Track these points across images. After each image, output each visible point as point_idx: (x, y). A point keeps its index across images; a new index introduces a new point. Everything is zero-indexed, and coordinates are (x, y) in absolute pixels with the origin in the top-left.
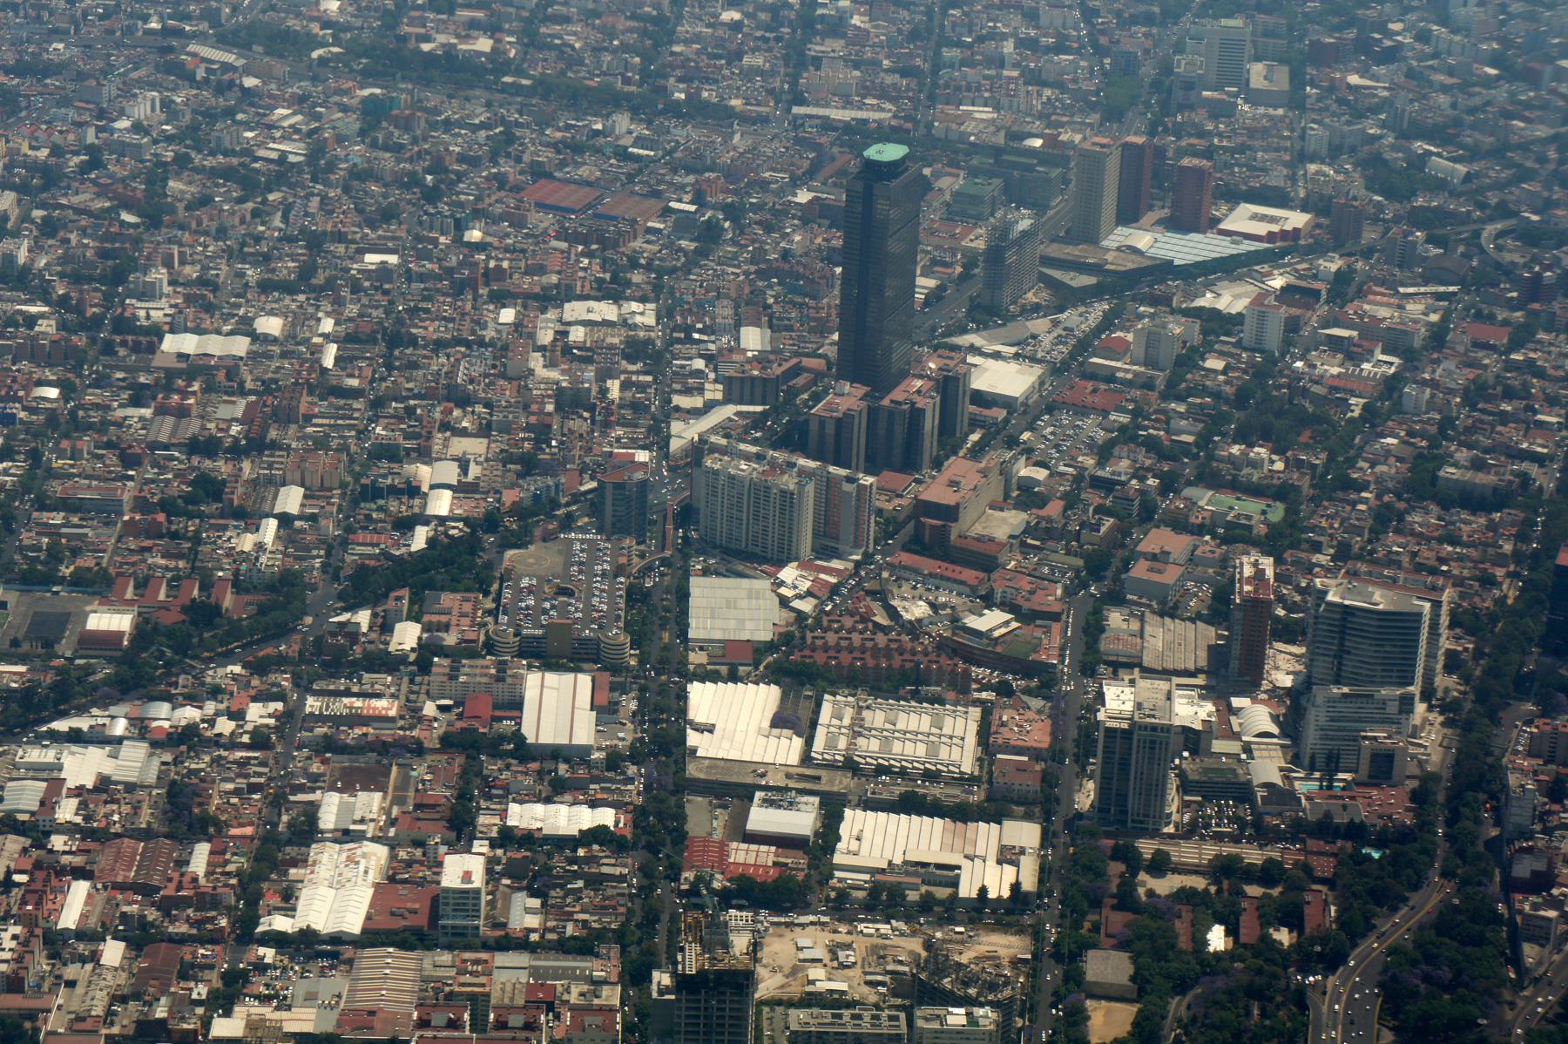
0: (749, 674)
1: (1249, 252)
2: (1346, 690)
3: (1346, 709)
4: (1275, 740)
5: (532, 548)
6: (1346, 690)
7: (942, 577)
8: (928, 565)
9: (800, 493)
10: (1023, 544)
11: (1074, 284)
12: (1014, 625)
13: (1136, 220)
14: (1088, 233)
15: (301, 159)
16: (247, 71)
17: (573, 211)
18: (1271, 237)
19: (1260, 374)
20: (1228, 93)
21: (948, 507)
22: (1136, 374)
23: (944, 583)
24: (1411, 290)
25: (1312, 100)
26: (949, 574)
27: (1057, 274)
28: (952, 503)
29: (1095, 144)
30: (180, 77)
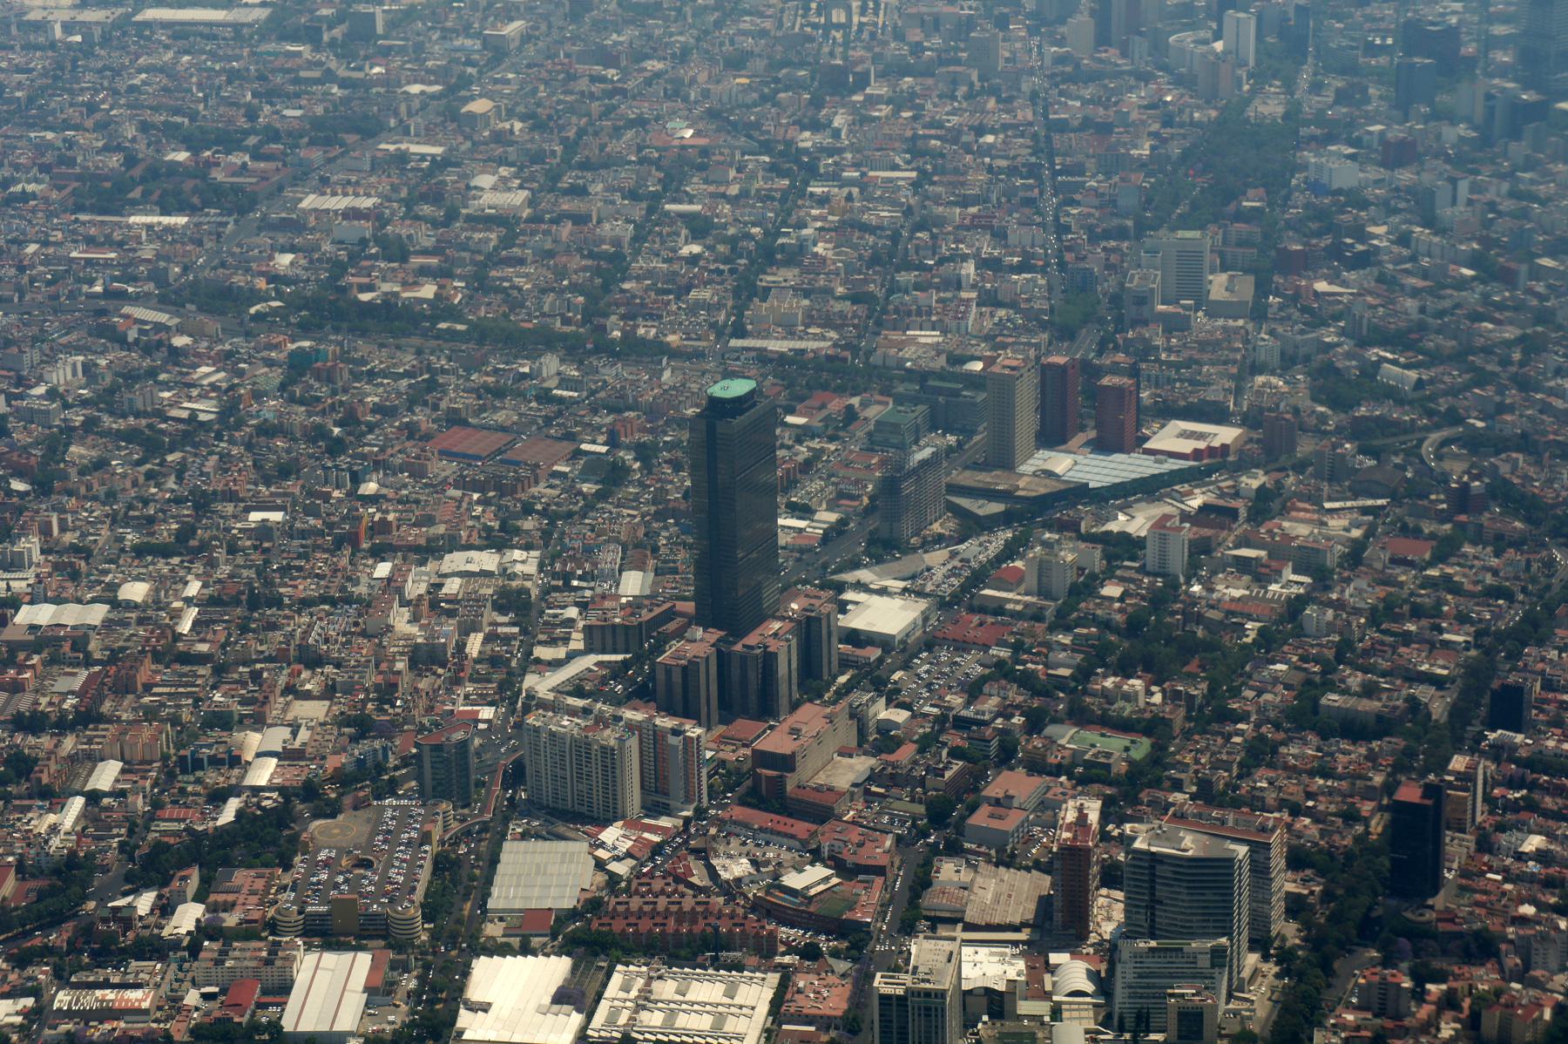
0: (545, 945)
1: (1180, 470)
2: (1153, 944)
3: (1152, 964)
4: (1088, 999)
5: (340, 817)
6: (1153, 944)
7: (772, 832)
8: (760, 818)
9: (621, 748)
10: (867, 792)
11: (981, 512)
12: (835, 880)
13: (1064, 442)
14: (1003, 459)
15: (212, 416)
17: (478, 458)
18: (1197, 454)
19: (1158, 601)
20: (1184, 307)
21: (783, 756)
22: (1027, 605)
24: (1337, 505)
25: (1275, 309)
26: (780, 828)
28: (788, 752)
30: (110, 339)
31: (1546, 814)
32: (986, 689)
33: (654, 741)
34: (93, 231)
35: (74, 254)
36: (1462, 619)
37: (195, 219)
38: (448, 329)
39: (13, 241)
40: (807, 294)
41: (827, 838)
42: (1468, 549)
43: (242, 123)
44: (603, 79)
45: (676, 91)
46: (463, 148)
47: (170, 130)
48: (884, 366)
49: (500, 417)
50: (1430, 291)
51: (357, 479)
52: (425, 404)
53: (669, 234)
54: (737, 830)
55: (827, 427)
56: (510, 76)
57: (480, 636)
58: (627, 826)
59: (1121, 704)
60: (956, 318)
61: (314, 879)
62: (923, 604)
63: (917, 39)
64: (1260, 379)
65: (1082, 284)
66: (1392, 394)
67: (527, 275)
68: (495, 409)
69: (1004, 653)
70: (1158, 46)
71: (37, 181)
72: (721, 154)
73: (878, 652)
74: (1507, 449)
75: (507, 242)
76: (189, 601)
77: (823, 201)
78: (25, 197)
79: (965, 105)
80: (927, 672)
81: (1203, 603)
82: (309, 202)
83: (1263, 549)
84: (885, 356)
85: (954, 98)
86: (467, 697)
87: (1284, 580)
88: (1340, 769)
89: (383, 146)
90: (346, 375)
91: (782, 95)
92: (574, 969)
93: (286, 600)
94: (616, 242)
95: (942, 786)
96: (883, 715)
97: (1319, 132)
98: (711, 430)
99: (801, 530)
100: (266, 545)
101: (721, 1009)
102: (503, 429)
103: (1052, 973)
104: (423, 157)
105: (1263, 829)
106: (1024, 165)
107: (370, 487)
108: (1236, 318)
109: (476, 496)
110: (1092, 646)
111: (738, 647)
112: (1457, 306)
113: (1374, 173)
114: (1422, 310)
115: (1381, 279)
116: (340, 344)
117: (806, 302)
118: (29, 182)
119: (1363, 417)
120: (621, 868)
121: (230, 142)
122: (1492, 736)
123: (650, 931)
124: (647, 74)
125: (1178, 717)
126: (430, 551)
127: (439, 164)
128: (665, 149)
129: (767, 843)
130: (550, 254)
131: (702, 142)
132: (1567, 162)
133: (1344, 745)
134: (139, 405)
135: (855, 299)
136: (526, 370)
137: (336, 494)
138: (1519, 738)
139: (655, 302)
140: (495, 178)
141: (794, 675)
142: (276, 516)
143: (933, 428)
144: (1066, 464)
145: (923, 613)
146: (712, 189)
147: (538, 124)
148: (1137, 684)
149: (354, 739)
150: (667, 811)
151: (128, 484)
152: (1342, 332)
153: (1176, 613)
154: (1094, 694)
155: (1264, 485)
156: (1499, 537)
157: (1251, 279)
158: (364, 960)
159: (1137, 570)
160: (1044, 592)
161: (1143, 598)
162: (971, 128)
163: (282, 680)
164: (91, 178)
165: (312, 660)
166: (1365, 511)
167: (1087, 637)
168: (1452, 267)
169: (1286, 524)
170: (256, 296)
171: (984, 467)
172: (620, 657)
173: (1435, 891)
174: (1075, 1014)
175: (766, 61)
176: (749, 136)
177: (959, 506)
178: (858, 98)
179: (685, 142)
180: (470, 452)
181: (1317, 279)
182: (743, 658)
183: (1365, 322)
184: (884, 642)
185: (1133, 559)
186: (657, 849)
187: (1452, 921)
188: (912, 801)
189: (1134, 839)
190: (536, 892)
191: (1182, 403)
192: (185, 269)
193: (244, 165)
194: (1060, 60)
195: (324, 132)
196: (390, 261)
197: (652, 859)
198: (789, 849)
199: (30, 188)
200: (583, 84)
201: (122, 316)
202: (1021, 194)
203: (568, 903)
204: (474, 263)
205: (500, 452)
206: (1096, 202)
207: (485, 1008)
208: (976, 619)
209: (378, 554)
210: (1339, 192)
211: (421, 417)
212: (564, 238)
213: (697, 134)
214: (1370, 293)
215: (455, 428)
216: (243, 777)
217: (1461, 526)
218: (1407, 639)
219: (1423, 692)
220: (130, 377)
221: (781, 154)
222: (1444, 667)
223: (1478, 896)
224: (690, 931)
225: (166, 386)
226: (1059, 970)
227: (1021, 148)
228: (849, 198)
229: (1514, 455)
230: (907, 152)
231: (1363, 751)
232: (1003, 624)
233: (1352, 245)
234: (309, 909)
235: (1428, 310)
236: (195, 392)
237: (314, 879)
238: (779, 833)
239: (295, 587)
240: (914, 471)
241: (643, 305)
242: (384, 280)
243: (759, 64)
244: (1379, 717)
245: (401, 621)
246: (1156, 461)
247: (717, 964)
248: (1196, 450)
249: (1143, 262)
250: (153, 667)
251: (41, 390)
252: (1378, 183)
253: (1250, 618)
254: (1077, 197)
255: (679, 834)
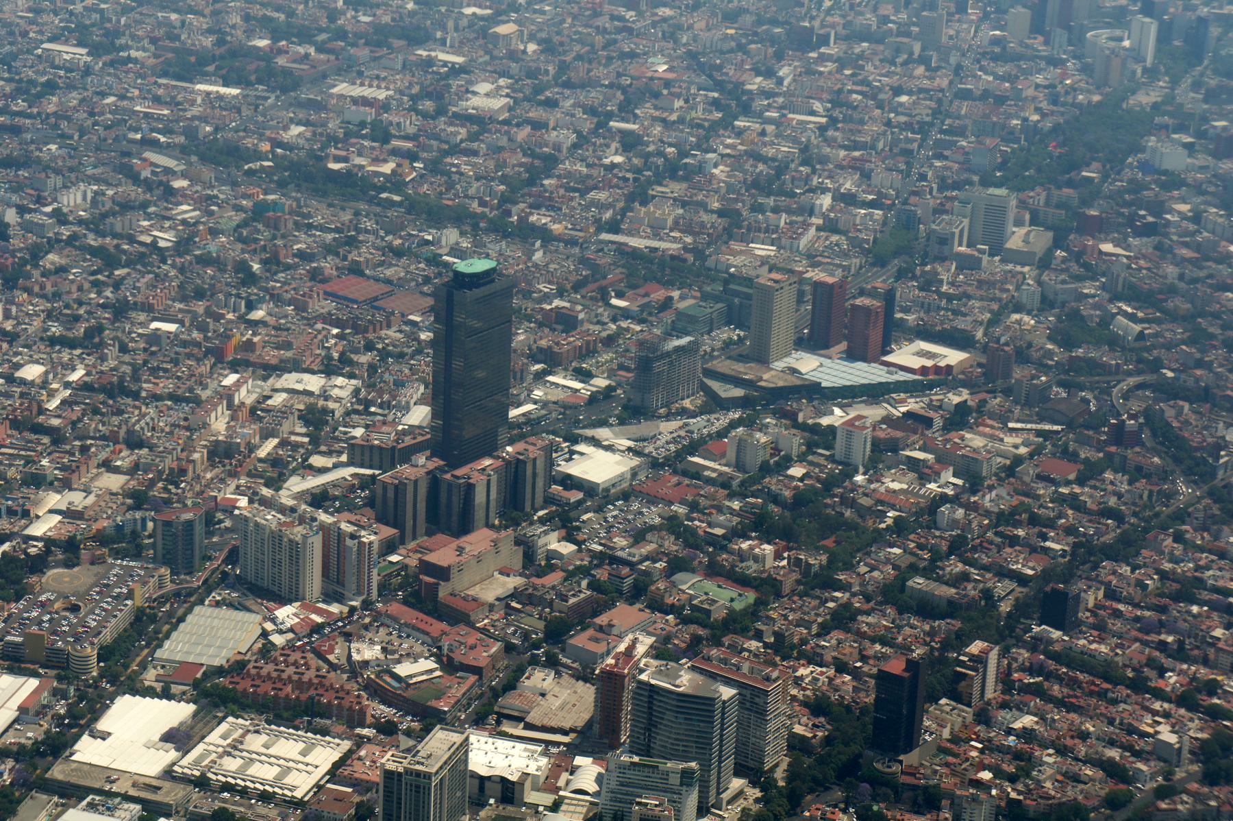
0: (184, 693)
1: (905, 382)
2: (636, 759)
3: (632, 775)
4: (588, 798)
5: (76, 569)
6: (636, 759)
7: (414, 628)
8: (410, 615)
9: (304, 543)
10: (508, 606)
11: (723, 395)
12: (438, 673)
13: (827, 347)
14: (761, 357)
15: (169, 244)
16: (184, 175)
17: (354, 301)
18: (924, 370)
19: (829, 485)
20: (979, 251)
21: (441, 568)
22: (721, 474)
23: (414, 633)
24: (1019, 425)
25: (1058, 261)
26: (422, 626)
27: (710, 382)
28: (446, 565)
29: (770, 279)
30: (126, 176)
31: (1048, 699)
32: (649, 536)
33: (333, 541)
34: (161, 92)
35: (138, 108)
36: (1070, 530)
37: (245, 93)
38: (387, 198)
39: (98, 93)
40: (684, 204)
41: (454, 638)
42: (1108, 475)
43: (324, 23)
44: (621, 19)
45: (671, 36)
46: (481, 60)
47: (265, 23)
48: (716, 270)
49: (389, 272)
50: (1195, 263)
51: (251, 306)
52: (337, 254)
53: (601, 145)
54: (388, 622)
55: (642, 311)
56: (547, 8)
57: (275, 441)
58: (303, 607)
59: (751, 563)
60: (791, 238)
61: (25, 615)
62: (636, 461)
63: (886, 13)
64: (1016, 316)
65: (908, 222)
66: (1114, 342)
67: (474, 165)
68: (391, 265)
69: (680, 510)
70: (1077, 39)
71: (144, 50)
72: (680, 87)
73: (580, 495)
74: (1176, 397)
75: (473, 137)
76: (67, 385)
77: (739, 133)
78: (129, 59)
79: (899, 70)
80: (615, 517)
81: (861, 491)
82: (342, 88)
83: (930, 453)
84: (717, 261)
85: (893, 63)
86: (238, 487)
87: (942, 480)
88: (900, 639)
89: (419, 52)
90: (290, 225)
91: (753, 46)
92: (195, 715)
93: (144, 394)
94: (557, 147)
95: (565, 610)
96: (554, 546)
97: (1171, 122)
98: (450, 298)
99: (578, 391)
100: (153, 349)
101: (291, 764)
102: (388, 281)
103: (572, 773)
104: (445, 64)
105: (768, 679)
106: (918, 122)
107: (258, 314)
108: (1023, 265)
109: (335, 331)
110: (754, 514)
111: (448, 476)
112: (1210, 276)
113: (1202, 160)
114: (1181, 277)
115: (1158, 247)
116: (297, 200)
117: (681, 211)
118: (138, 50)
119: (1077, 357)
120: (278, 640)
121: (305, 36)
122: (1036, 629)
123: (245, 690)
124: (657, 18)
125: (789, 581)
126: (270, 370)
127: (456, 71)
128: (638, 78)
129: (408, 636)
130: (500, 149)
131: (671, 76)
132: (1228, 156)
133: (914, 621)
134: (118, 228)
135: (721, 213)
136: (430, 238)
137: (230, 316)
138: (1056, 634)
139: (563, 197)
140: (493, 87)
141: (493, 504)
142: (171, 327)
143: (728, 323)
144: (809, 365)
145: (632, 469)
146: (657, 113)
147: (548, 47)
148: (768, 548)
149: (130, 508)
150: (339, 598)
151: (74, 288)
152: (1103, 287)
153: (836, 496)
154: (731, 553)
155: (966, 401)
156: (1139, 469)
157: (1050, 234)
158: (33, 683)
159: (827, 458)
160: (739, 466)
161: (818, 480)
162: (892, 88)
163: (103, 455)
164: (184, 52)
165: (134, 442)
166: (1039, 433)
167: (753, 505)
168: (1224, 243)
169: (968, 436)
170: (260, 156)
171: (742, 358)
172: (368, 472)
173: (908, 748)
174: (572, 808)
175: (754, 18)
176: (710, 76)
177: (710, 388)
178: (814, 55)
179: (656, 75)
180: (350, 296)
181: (1106, 241)
182: (450, 485)
183: (1121, 281)
184: (588, 489)
185: (827, 448)
186: (317, 629)
187: (913, 775)
188: (540, 618)
189: (642, 671)
190: (212, 651)
191: (938, 328)
192: (217, 129)
193: (307, 56)
194: (996, 41)
195: (378, 38)
196: (374, 141)
197: (310, 635)
198: (423, 644)
199: (134, 54)
200: (604, 22)
201: (140, 159)
202: (902, 145)
203: (217, 662)
204: (440, 150)
205: (376, 299)
206: (961, 159)
207: (104, 736)
208: (675, 479)
209: (234, 367)
210: (1165, 173)
211: (328, 265)
212: (519, 139)
213: (670, 70)
214: (1144, 257)
215: (351, 276)
216: (27, 526)
217: (1110, 456)
218: (1013, 541)
219: (1001, 587)
220: (125, 206)
221: (730, 93)
222: (1033, 569)
223: (950, 759)
224: (297, 698)
225: (148, 217)
226: (578, 772)
227: (924, 112)
228: (763, 133)
229: (1181, 403)
230: (829, 101)
231: (927, 628)
232: (696, 487)
233: (1144, 217)
234: (9, 638)
235: (1187, 278)
236: (167, 224)
237: (25, 615)
238: (418, 630)
239: (156, 384)
240: (668, 354)
241: (550, 199)
242: (360, 155)
243: (748, 19)
244: (950, 602)
245: (219, 423)
246: (888, 372)
247: (311, 728)
248: (923, 367)
249: (955, 210)
250: (9, 432)
251: (48, 209)
252: (1203, 169)
253: (893, 507)
254: (946, 153)
255: (341, 619)
